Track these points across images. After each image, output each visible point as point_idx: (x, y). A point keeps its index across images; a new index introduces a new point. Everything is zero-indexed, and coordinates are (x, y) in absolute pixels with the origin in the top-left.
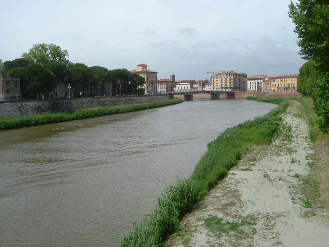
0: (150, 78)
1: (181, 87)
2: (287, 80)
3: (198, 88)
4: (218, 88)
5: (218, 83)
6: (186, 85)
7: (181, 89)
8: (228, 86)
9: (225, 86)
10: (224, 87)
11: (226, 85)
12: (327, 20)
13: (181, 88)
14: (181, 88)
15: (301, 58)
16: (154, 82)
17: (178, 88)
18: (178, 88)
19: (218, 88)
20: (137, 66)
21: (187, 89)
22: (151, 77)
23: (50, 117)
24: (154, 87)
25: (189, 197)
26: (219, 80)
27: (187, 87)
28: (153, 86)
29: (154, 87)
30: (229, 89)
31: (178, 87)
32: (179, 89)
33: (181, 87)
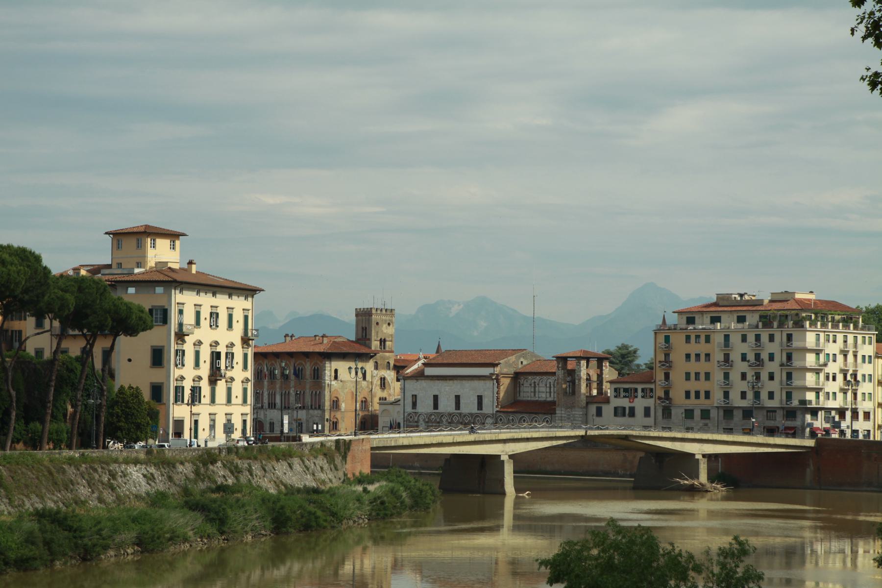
0: (198, 323)
1: (436, 398)
2: (403, 427)
3: (553, 403)
4: (697, 414)
5: (697, 375)
6: (467, 384)
7: (474, 410)
8: (771, 395)
9: (750, 395)
10: (744, 404)
11: (757, 395)
12: (1, 500)
13: (436, 406)
14: (436, 406)
15: (632, 346)
16: (230, 356)
17: (414, 405)
18: (414, 405)
19: (697, 414)
20: (109, 238)
21: (474, 410)
22: (205, 323)
23: (376, 396)
24: (229, 390)
25: (96, 405)
26: (708, 356)
27: (480, 398)
28: (221, 386)
29: (229, 390)
30: (121, 460)
31: (415, 397)
32: (420, 409)
33: (436, 398)
